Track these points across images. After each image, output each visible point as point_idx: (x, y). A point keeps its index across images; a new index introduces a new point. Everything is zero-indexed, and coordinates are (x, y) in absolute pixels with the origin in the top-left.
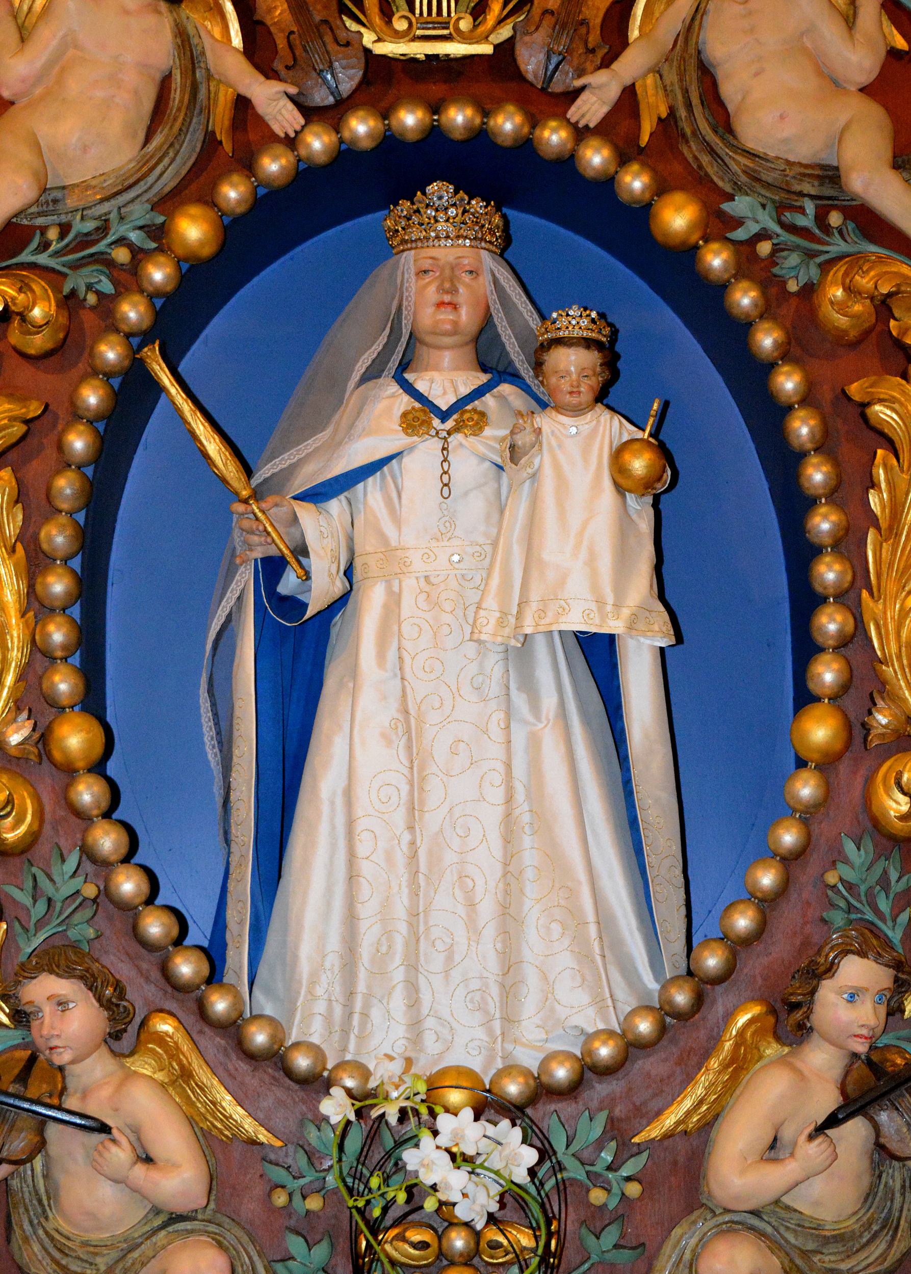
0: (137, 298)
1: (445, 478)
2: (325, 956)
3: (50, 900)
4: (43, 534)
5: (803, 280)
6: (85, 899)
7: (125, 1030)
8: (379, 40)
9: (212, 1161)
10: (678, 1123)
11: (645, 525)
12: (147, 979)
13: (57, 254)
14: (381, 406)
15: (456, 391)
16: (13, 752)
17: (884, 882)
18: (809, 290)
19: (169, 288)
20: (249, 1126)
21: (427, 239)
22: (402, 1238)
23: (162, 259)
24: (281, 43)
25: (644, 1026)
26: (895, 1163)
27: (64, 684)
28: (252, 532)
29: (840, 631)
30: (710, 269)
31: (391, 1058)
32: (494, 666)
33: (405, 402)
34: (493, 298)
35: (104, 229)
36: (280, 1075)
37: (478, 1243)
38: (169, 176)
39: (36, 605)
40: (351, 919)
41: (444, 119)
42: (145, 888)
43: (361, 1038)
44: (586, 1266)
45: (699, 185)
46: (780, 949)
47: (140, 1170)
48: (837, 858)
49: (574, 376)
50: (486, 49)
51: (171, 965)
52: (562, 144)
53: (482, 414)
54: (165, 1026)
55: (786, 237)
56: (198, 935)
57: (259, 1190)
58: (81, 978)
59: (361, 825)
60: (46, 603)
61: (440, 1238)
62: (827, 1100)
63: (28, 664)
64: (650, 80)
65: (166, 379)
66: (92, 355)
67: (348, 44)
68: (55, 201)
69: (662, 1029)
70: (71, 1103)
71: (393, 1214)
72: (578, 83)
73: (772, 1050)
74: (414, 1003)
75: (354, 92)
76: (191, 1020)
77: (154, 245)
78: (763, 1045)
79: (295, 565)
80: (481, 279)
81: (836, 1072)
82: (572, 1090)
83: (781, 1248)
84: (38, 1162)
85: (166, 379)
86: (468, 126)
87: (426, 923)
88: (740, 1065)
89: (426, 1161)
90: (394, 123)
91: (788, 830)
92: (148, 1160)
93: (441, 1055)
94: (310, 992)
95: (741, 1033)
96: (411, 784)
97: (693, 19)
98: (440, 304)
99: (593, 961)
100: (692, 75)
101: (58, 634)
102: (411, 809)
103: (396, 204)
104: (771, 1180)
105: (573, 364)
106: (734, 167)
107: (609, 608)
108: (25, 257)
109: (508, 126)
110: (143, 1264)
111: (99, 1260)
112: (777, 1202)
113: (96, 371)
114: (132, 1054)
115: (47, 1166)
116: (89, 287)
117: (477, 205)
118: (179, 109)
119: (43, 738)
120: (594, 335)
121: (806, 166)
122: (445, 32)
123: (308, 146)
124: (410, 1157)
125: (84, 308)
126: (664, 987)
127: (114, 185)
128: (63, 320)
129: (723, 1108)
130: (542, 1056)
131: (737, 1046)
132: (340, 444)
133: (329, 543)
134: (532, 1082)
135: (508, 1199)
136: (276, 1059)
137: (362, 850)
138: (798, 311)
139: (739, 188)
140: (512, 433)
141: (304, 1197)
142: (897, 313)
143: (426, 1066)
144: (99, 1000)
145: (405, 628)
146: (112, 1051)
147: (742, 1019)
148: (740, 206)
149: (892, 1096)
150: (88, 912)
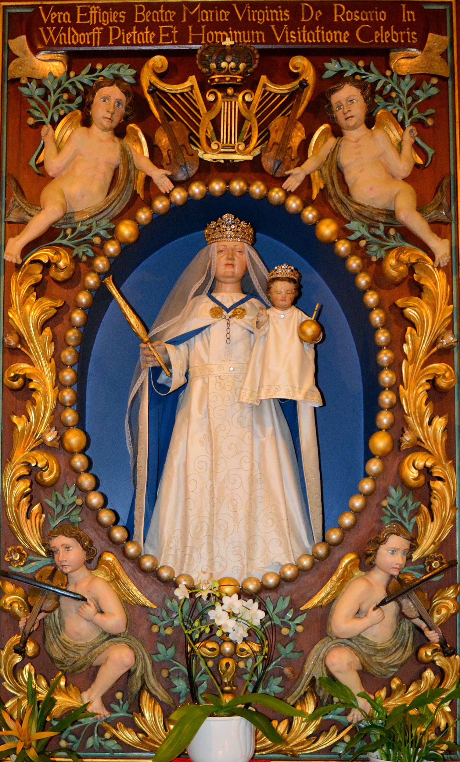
0: (103, 258)
1: (228, 336)
2: (174, 531)
3: (63, 505)
4: (62, 355)
5: (379, 256)
6: (77, 505)
7: (92, 559)
8: (205, 153)
9: (128, 613)
10: (319, 602)
11: (311, 356)
12: (102, 539)
13: (70, 240)
14: (202, 306)
15: (233, 300)
16: (49, 445)
17: (406, 505)
18: (380, 261)
19: (116, 255)
20: (143, 600)
21: (222, 238)
22: (205, 646)
23: (113, 242)
24: (165, 154)
25: (306, 562)
26: (406, 620)
27: (70, 416)
28: (147, 356)
29: (391, 402)
30: (339, 251)
31: (204, 573)
32: (247, 413)
33: (212, 304)
34: (249, 262)
35: (89, 230)
36: (156, 579)
37: (235, 650)
38: (117, 211)
39: (59, 384)
40: (186, 516)
41: (231, 187)
42: (102, 501)
43: (189, 565)
44: (279, 659)
45: (336, 216)
46: (362, 532)
47: (99, 616)
48: (387, 494)
49: (284, 293)
50: (250, 158)
51: (112, 533)
52: (280, 198)
53: (244, 310)
54: (109, 558)
55: (372, 238)
56: (124, 520)
57: (146, 626)
58: (76, 537)
59: (190, 478)
60: (63, 383)
61: (220, 646)
62: (381, 594)
63: (56, 409)
64: (316, 173)
65: (114, 291)
66: (84, 281)
67: (192, 155)
68: (70, 218)
69: (313, 564)
70: (71, 588)
71: (204, 637)
72: (287, 173)
73: (358, 573)
74: (211, 551)
75: (195, 175)
76: (120, 556)
77: (110, 237)
78: (354, 571)
79: (166, 370)
80: (244, 255)
81: (384, 583)
82: (275, 588)
83: (360, 653)
84: (57, 612)
85: (114, 291)
86: (241, 190)
87: (217, 518)
88: (345, 579)
89: (218, 616)
90: (210, 188)
91: (367, 483)
92: (102, 612)
93: (222, 572)
94: (168, 546)
95: (346, 566)
96: (212, 461)
97: (335, 149)
98: (227, 265)
99: (285, 535)
100: (334, 171)
101: (68, 396)
102: (212, 471)
103: (210, 223)
104: (357, 626)
105: (283, 289)
106: (351, 209)
107: (297, 389)
108: (57, 241)
109: (257, 191)
110: (99, 654)
111: (81, 652)
112: (359, 635)
113: (85, 288)
114: (95, 569)
115: (60, 613)
116: (84, 253)
117: (243, 224)
118: (122, 180)
119: (61, 439)
120: (292, 277)
121: (381, 210)
122: (233, 150)
123: (175, 197)
124: (211, 614)
125: (81, 262)
126: (314, 547)
127: (95, 211)
128: (73, 267)
129: (337, 597)
130: (263, 574)
131: (344, 571)
132: (184, 322)
133: (180, 362)
134: (259, 584)
135: (251, 632)
136: (154, 573)
137: (191, 487)
138: (376, 269)
139: (353, 218)
140: (258, 316)
141: (165, 629)
142: (416, 271)
143: (217, 577)
144: (83, 546)
145: (210, 397)
146: (87, 568)
147: (346, 560)
148: (353, 225)
149: (408, 593)
150: (78, 511)
